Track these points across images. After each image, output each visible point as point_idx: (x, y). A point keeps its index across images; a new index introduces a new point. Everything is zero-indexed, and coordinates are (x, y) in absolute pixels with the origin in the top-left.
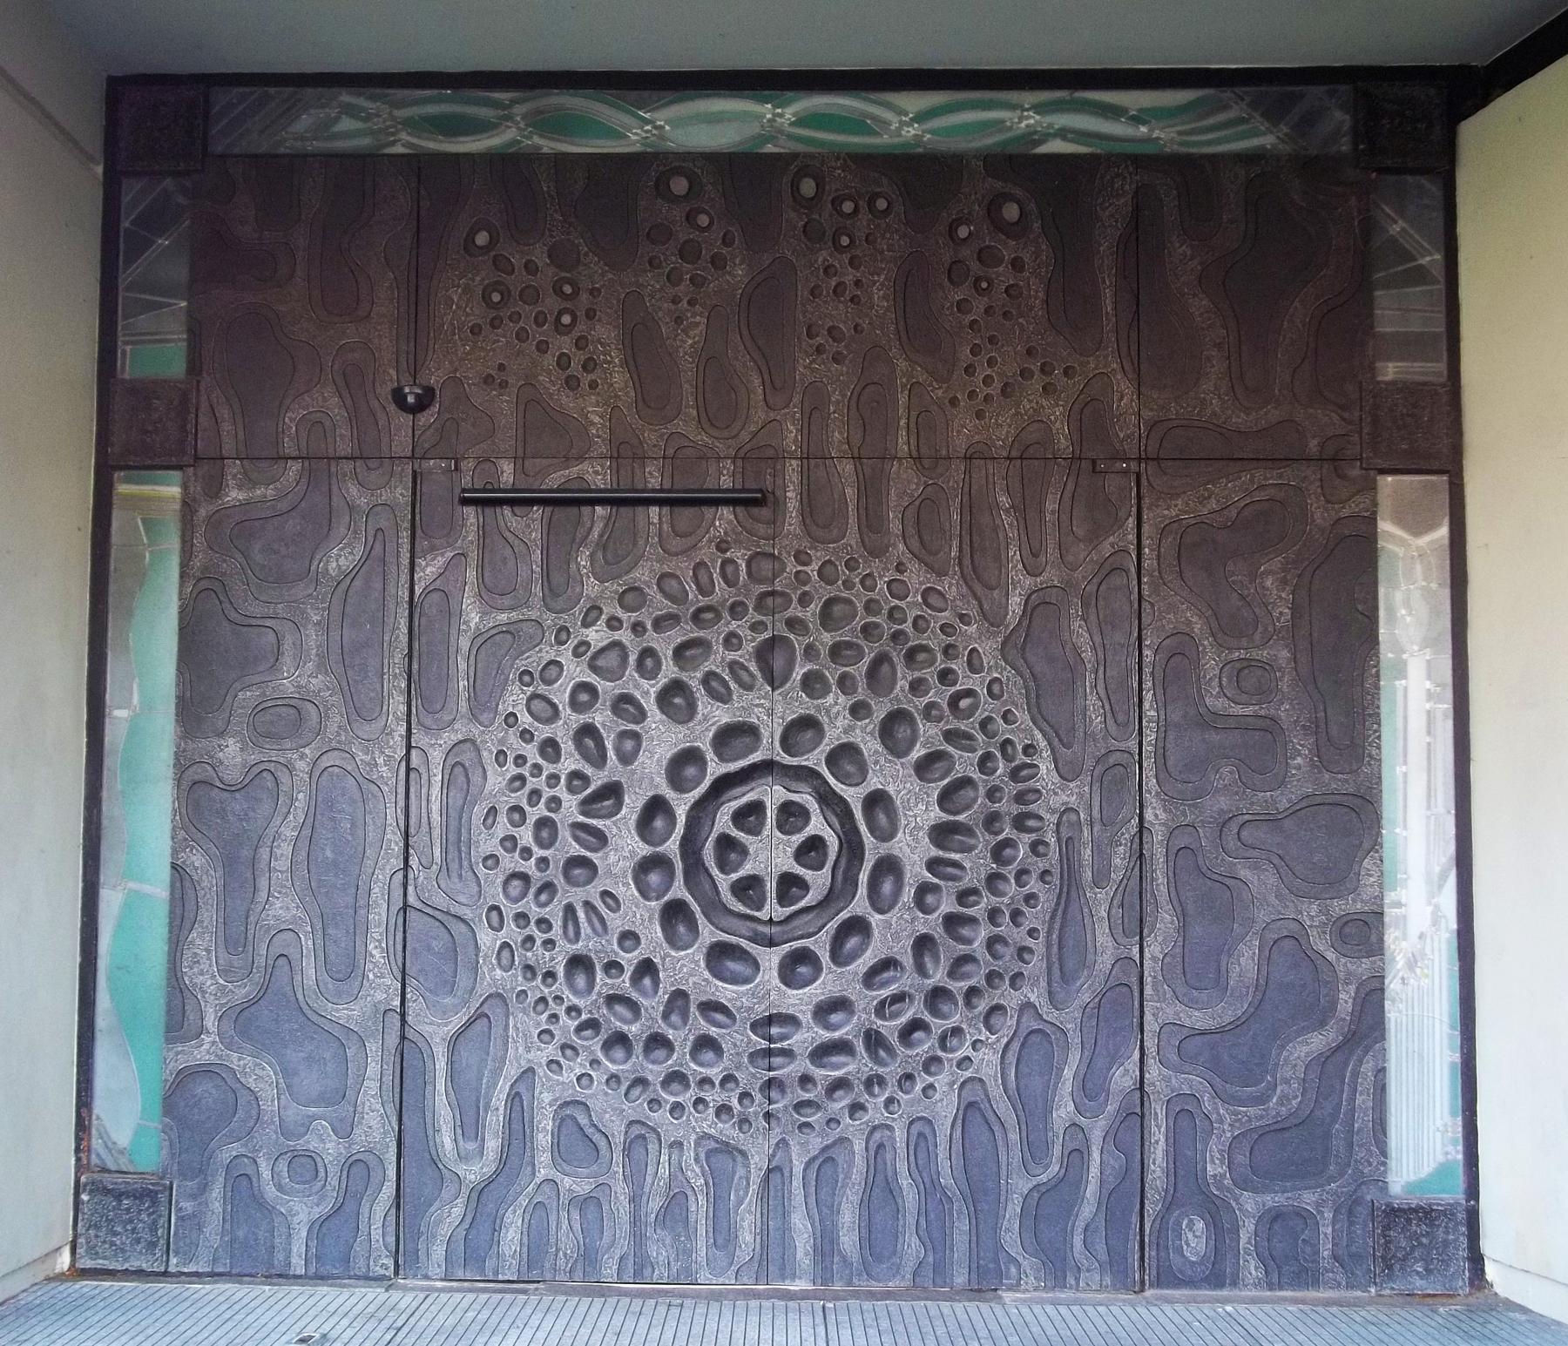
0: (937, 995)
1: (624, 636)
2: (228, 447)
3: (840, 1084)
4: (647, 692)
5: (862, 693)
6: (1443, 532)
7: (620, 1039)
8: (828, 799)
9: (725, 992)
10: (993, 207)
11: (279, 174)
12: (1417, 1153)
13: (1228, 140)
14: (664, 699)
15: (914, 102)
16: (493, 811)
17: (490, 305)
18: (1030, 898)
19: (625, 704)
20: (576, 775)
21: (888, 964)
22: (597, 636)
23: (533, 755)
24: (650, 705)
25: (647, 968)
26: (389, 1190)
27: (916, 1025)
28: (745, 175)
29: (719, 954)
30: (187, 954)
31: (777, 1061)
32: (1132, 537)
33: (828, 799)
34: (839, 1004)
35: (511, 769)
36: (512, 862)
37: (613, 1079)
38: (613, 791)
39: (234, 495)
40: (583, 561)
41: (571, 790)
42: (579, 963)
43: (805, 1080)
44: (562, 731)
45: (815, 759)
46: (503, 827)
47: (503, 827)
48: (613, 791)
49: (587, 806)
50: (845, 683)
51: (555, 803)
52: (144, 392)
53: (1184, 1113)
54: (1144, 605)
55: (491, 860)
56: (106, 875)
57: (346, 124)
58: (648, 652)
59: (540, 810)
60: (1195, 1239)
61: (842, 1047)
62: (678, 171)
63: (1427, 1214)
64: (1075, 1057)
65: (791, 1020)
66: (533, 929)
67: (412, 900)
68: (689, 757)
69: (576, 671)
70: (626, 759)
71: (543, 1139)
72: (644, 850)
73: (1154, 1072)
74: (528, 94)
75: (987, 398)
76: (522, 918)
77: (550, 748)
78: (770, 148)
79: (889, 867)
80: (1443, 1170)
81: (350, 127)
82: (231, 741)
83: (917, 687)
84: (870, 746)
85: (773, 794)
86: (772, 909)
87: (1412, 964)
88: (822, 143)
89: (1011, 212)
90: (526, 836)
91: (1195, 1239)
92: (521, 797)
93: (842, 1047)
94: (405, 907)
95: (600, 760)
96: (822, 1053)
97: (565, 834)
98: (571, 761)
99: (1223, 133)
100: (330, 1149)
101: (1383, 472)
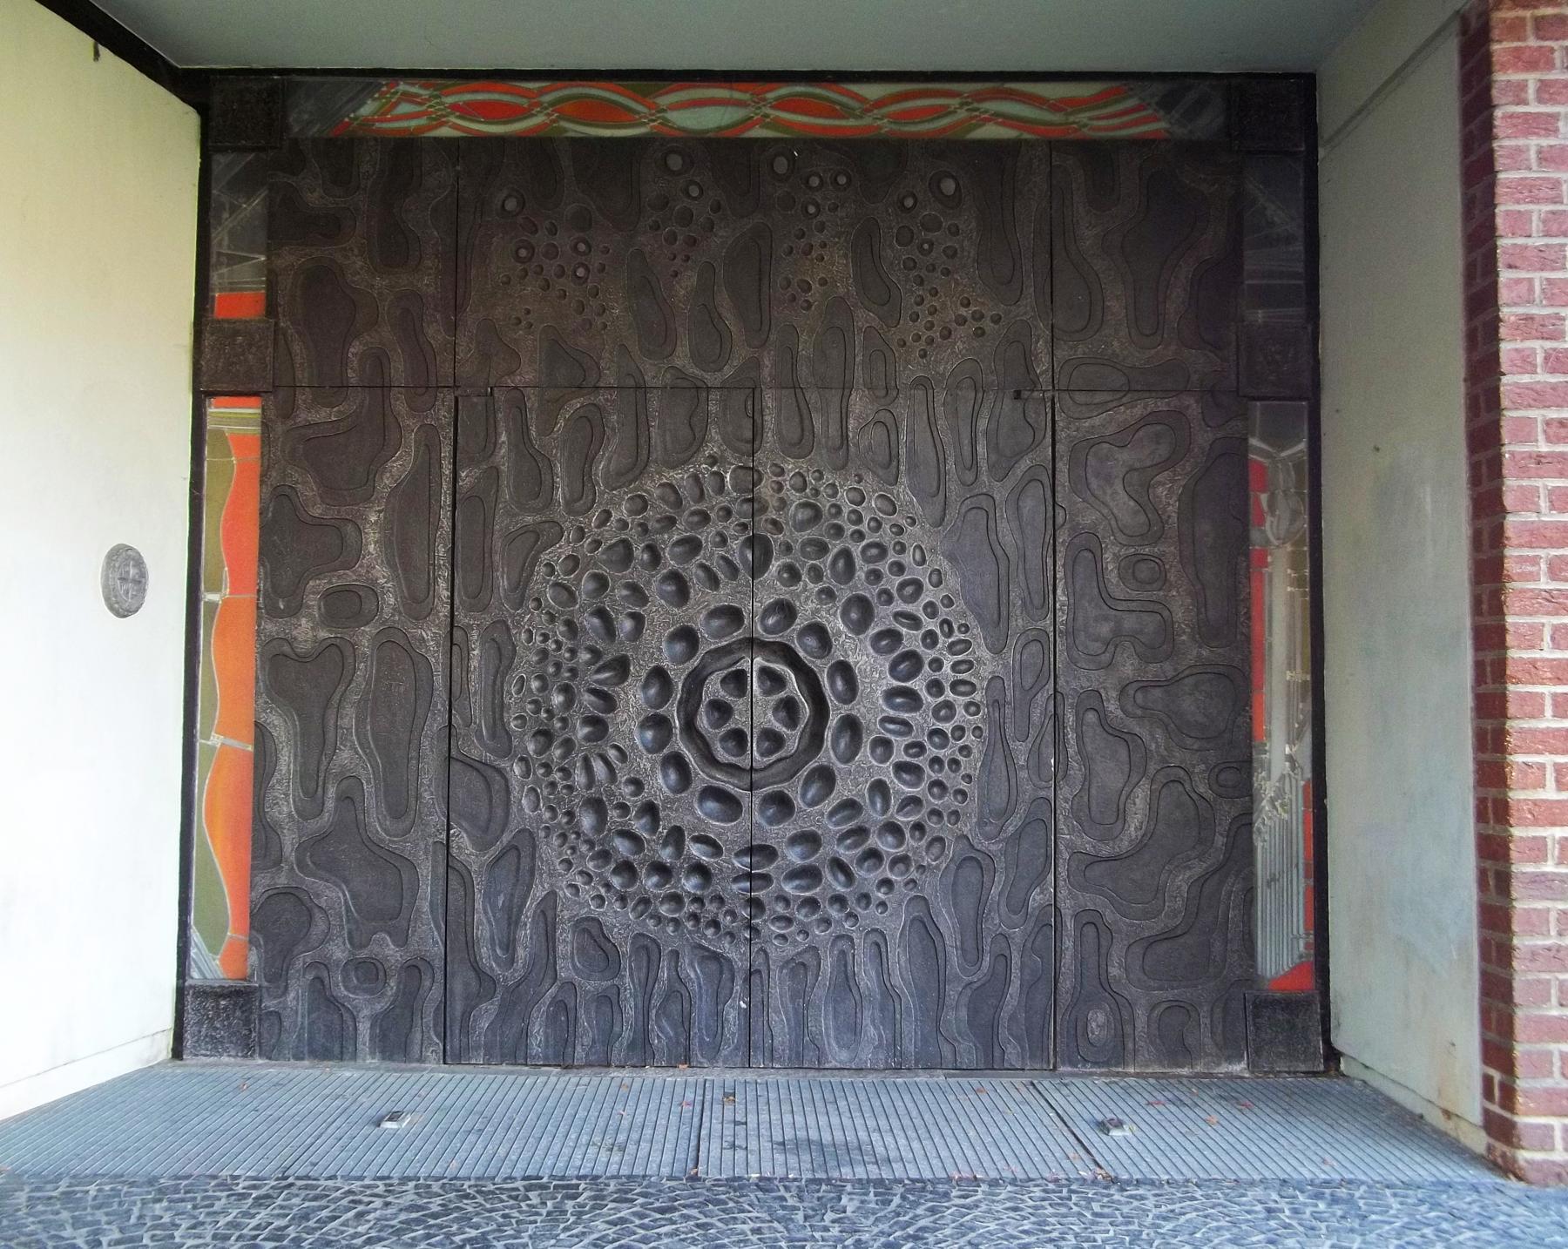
2: (303, 376)
5: (828, 581)
6: (1303, 446)
10: (935, 185)
11: (341, 152)
12: (1278, 953)
13: (1136, 123)
17: (518, 259)
18: (965, 750)
28: (726, 155)
30: (269, 798)
31: (757, 883)
32: (1061, 435)
39: (303, 416)
50: (817, 574)
52: (229, 332)
53: (1089, 921)
54: (1058, 510)
57: (405, 108)
60: (1098, 1021)
62: (673, 151)
64: (1000, 878)
67: (453, 753)
73: (1063, 893)
74: (558, 84)
75: (931, 341)
78: (757, 132)
79: (851, 726)
81: (405, 114)
82: (304, 621)
83: (876, 576)
84: (836, 624)
86: (756, 755)
88: (789, 125)
89: (949, 186)
91: (1098, 1021)
99: (1136, 115)
100: (391, 952)
101: (1254, 399)
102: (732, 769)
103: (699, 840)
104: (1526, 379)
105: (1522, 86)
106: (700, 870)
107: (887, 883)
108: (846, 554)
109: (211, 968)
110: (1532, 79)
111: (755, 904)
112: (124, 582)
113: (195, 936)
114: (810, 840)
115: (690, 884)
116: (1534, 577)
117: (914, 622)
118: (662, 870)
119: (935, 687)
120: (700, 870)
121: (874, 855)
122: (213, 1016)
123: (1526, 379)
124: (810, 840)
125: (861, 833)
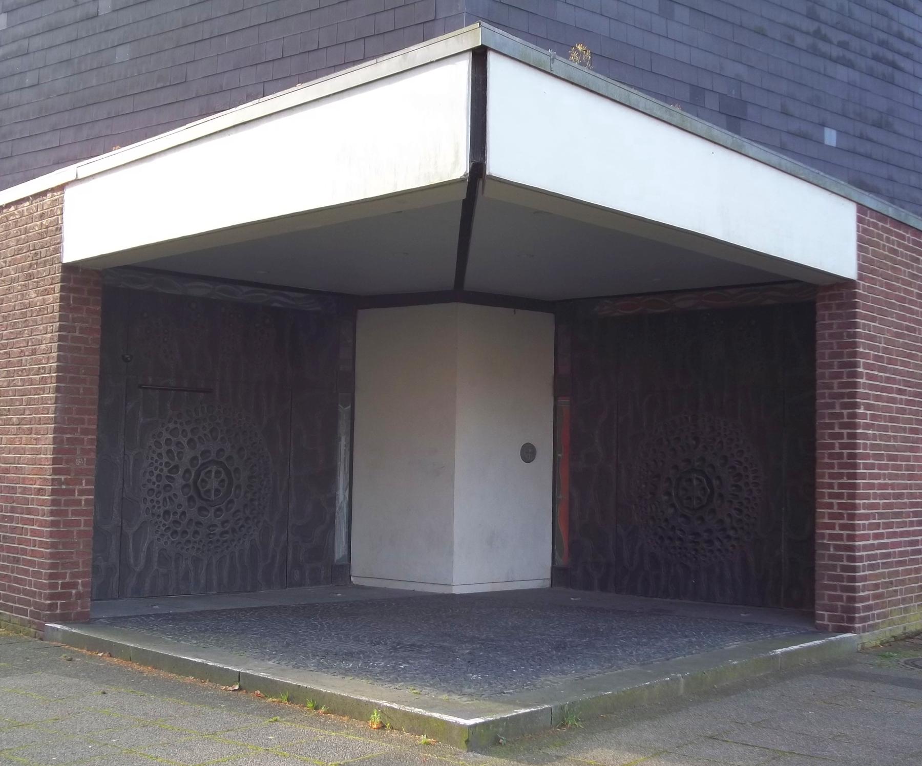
0: (247, 519)
1: (178, 426)
3: (225, 541)
4: (184, 441)
7: (175, 532)
8: (226, 469)
9: (201, 519)
12: (340, 551)
14: (188, 443)
15: (246, 289)
16: (145, 472)
19: (178, 444)
20: (167, 463)
21: (238, 511)
22: (171, 426)
23: (156, 458)
24: (185, 444)
25: (184, 513)
26: (117, 575)
27: (242, 526)
29: (201, 509)
33: (226, 469)
34: (227, 521)
35: (150, 461)
36: (150, 486)
37: (173, 542)
38: (176, 467)
40: (169, 405)
41: (166, 466)
42: (167, 513)
43: (218, 541)
44: (163, 450)
45: (223, 459)
46: (148, 476)
47: (148, 476)
48: (176, 467)
49: (169, 471)
51: (161, 470)
55: (144, 485)
56: (354, 477)
58: (184, 430)
59: (158, 472)
61: (227, 532)
63: (342, 566)
65: (215, 526)
66: (155, 503)
68: (195, 458)
69: (166, 435)
70: (180, 459)
71: (155, 559)
72: (184, 483)
76: (152, 501)
77: (160, 455)
80: (344, 556)
85: (214, 468)
87: (340, 508)
90: (154, 479)
92: (152, 468)
93: (227, 532)
94: (123, 498)
95: (173, 459)
96: (222, 534)
97: (164, 478)
98: (165, 459)
102: (206, 500)
103: (681, 530)
104: (823, 401)
105: (824, 315)
106: (680, 539)
107: (733, 546)
108: (721, 442)
109: (561, 562)
110: (826, 313)
111: (696, 550)
112: (528, 453)
113: (557, 554)
114: (709, 531)
115: (678, 543)
116: (823, 458)
117: (740, 463)
118: (670, 538)
119: (747, 484)
120: (680, 539)
121: (729, 537)
122: (559, 574)
123: (823, 401)
124: (709, 531)
125: (724, 530)
